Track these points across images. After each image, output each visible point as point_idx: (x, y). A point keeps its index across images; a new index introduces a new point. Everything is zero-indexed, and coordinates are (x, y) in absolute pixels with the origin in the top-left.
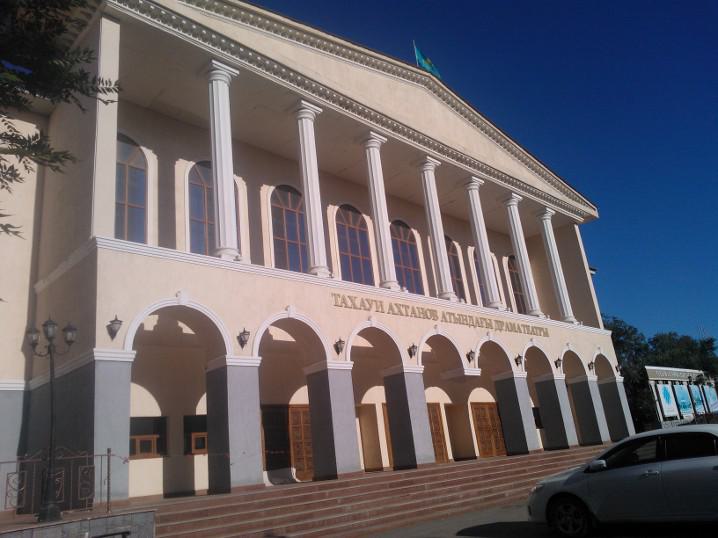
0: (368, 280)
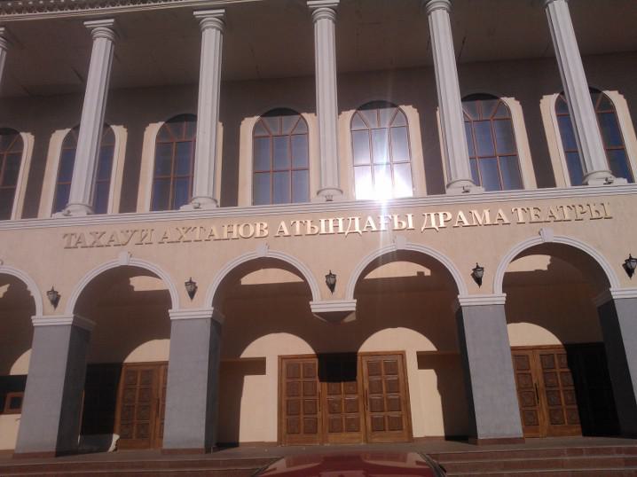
0: (554, 185)
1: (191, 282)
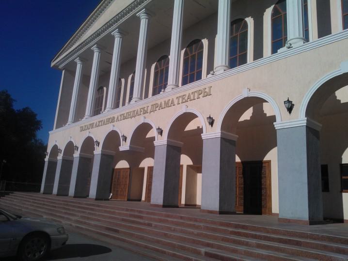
1: (210, 117)
